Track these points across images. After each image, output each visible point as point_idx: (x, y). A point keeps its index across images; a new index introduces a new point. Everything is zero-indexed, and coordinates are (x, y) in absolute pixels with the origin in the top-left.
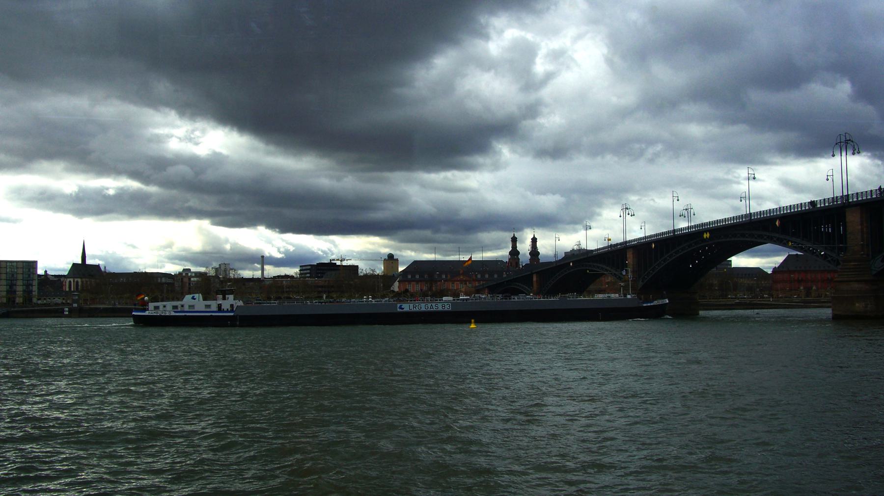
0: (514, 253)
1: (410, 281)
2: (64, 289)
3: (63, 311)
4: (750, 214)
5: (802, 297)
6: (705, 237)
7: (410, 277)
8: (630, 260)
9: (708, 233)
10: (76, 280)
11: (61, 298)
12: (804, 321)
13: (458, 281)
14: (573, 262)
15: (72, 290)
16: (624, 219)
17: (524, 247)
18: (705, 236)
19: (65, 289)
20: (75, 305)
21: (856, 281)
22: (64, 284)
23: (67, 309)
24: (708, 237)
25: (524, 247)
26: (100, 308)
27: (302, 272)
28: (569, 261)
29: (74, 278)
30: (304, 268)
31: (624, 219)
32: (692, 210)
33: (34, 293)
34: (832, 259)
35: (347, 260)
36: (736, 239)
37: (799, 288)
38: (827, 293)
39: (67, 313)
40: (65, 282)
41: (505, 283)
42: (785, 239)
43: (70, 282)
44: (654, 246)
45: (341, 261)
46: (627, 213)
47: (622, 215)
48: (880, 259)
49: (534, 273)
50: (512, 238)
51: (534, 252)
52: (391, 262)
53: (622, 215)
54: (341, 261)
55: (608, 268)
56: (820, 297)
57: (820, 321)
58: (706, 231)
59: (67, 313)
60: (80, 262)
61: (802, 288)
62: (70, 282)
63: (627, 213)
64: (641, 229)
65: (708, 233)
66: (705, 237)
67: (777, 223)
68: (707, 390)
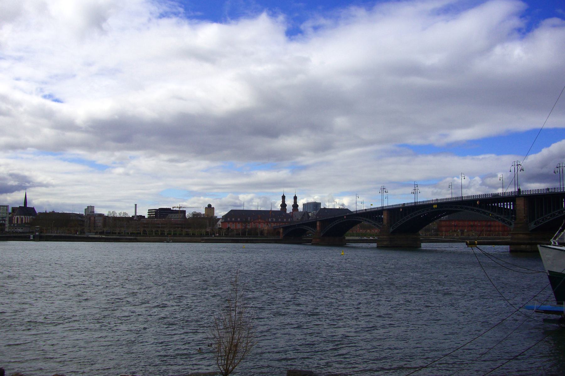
0: (284, 205)
1: (229, 222)
2: (13, 222)
3: (30, 237)
4: (462, 197)
5: (459, 236)
6: (434, 207)
7: (229, 219)
8: (384, 216)
9: (436, 205)
10: (21, 216)
11: (21, 228)
12: (367, 248)
13: (258, 222)
14: (346, 216)
15: (19, 223)
16: (382, 194)
17: (289, 202)
18: (434, 206)
19: (14, 222)
20: (37, 234)
21: (522, 234)
22: (14, 219)
23: (32, 236)
24: (436, 207)
25: (289, 202)
26: (52, 236)
27: (149, 213)
28: (344, 215)
29: (20, 215)
30: (150, 211)
31: (382, 194)
32: (418, 190)
33: (6, 225)
34: (501, 219)
35: (183, 208)
36: (452, 209)
37: (457, 230)
38: (473, 234)
39: (32, 238)
40: (14, 218)
41: (297, 226)
42: (481, 211)
43: (18, 218)
44: (401, 210)
45: (180, 208)
46: (384, 191)
47: (381, 192)
48: (534, 223)
49: (318, 221)
50: (282, 197)
51: (295, 206)
52: (210, 209)
53: (381, 192)
54: (180, 208)
55: (369, 220)
56: (469, 236)
57: (372, 248)
58: (435, 204)
59: (32, 238)
60: (23, 206)
61: (459, 230)
62: (18, 218)
63: (384, 191)
64: (386, 198)
65: (436, 205)
66: (434, 207)
67: (478, 203)
68: (351, 308)
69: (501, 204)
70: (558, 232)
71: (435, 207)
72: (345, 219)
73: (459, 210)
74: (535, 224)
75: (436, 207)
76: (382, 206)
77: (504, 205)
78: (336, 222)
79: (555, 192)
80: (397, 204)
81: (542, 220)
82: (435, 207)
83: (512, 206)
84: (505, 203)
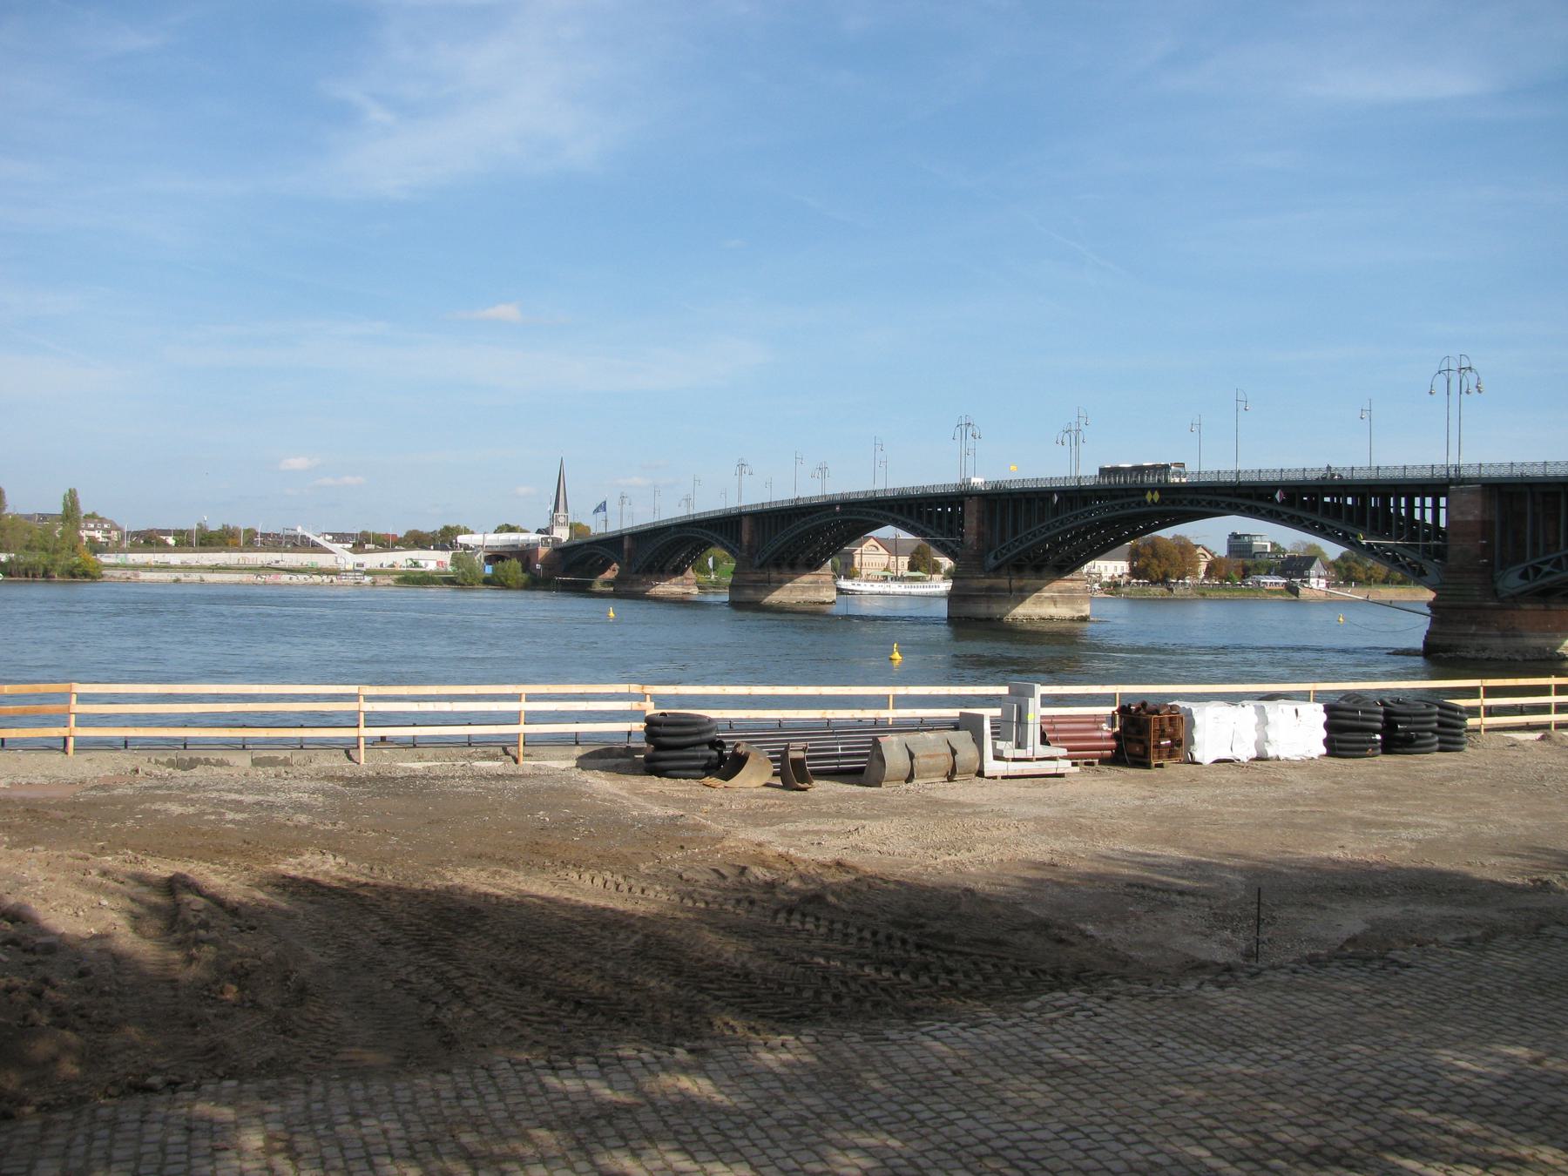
9: (1156, 493)
18: (1149, 497)
24: (1149, 492)
44: (1056, 498)
47: (958, 437)
48: (1520, 572)
65: (1156, 493)
69: (1423, 502)
70: (550, 763)
71: (1153, 494)
72: (836, 514)
73: (1203, 509)
74: (1524, 576)
75: (1149, 492)
76: (1073, 475)
77: (1410, 507)
78: (1129, 505)
79: (1065, 487)
80: (936, 483)
81: (1552, 562)
82: (1153, 494)
83: (1443, 513)
84: (1417, 501)
